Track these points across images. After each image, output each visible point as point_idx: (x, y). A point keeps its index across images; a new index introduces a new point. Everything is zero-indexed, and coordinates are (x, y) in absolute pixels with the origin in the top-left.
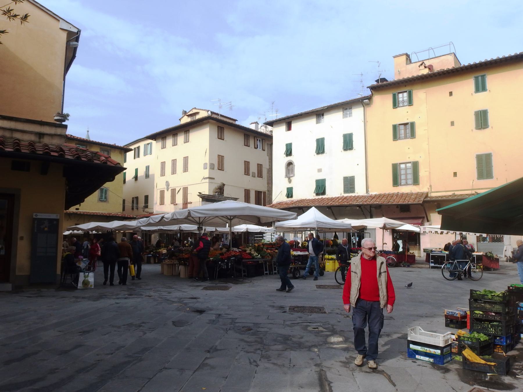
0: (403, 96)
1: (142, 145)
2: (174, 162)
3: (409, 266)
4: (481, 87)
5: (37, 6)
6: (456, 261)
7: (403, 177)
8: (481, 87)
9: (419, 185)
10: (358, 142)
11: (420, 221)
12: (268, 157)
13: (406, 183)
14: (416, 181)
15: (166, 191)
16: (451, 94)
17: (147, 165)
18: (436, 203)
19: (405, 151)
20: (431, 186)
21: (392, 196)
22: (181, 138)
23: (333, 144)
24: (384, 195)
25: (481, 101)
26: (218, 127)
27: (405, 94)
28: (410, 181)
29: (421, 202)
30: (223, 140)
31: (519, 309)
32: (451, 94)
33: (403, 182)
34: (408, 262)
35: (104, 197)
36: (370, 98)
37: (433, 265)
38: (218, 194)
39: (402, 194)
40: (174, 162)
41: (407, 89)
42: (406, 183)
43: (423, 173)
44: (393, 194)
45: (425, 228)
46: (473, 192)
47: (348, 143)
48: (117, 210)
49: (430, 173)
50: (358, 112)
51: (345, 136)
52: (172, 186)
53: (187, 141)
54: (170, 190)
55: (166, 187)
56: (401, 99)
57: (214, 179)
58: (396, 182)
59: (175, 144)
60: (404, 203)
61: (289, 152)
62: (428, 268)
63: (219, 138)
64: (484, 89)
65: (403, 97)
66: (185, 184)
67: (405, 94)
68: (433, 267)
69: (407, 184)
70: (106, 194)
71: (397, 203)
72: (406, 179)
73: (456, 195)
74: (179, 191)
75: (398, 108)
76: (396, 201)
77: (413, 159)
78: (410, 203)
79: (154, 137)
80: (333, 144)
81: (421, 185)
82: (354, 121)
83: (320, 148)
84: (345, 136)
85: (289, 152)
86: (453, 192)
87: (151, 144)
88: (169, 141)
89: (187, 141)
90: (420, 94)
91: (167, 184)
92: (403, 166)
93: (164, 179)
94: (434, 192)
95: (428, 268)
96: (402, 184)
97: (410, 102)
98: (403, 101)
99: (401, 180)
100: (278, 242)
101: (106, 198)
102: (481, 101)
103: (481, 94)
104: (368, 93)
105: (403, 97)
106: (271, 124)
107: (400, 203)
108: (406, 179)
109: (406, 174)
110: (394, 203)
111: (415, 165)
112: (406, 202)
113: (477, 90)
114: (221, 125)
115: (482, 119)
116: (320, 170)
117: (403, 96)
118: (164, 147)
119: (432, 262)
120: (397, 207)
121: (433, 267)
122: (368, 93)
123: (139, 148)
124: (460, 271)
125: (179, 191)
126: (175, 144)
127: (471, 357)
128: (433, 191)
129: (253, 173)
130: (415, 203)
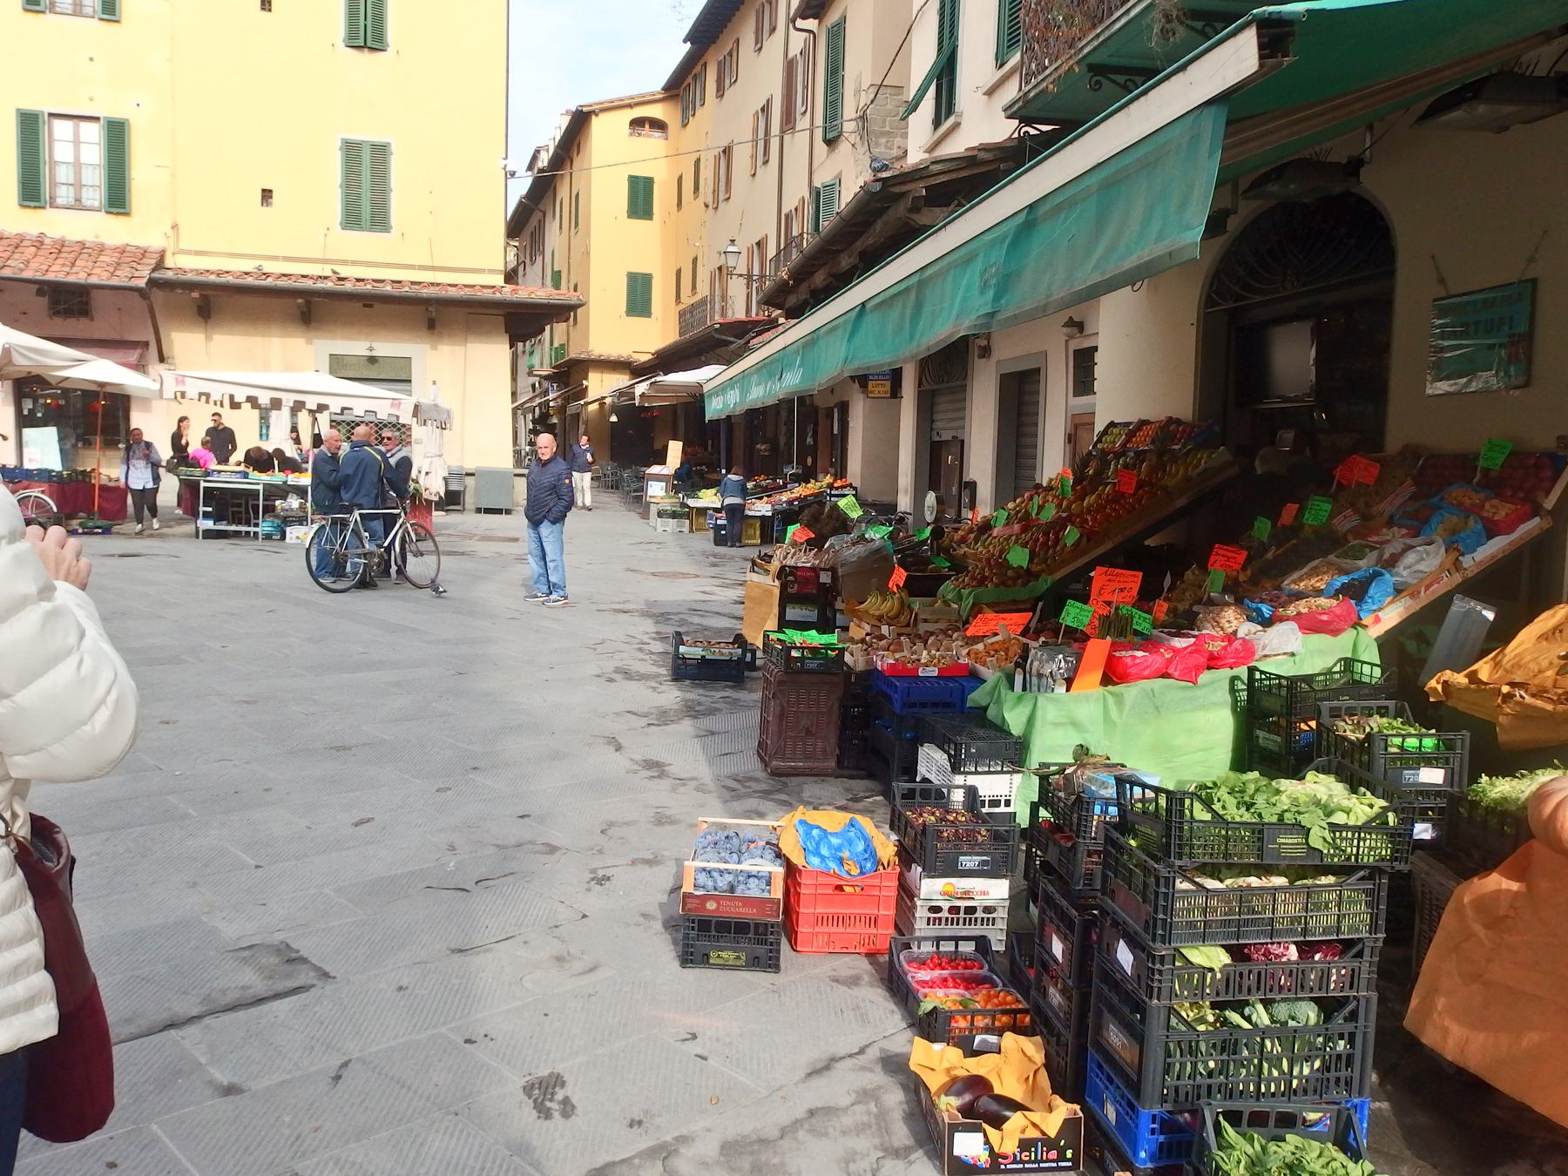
3: (107, 531)
6: (356, 514)
9: (127, 214)
11: (134, 356)
14: (117, 199)
18: (195, 295)
28: (95, 195)
29: (142, 283)
31: (1097, 809)
33: (64, 195)
34: (104, 514)
37: (209, 524)
38: (799, 785)
42: (78, 200)
44: (21, 238)
45: (181, 380)
46: (326, 270)
58: (32, 191)
60: (71, 279)
62: (188, 536)
68: (209, 535)
69: (78, 205)
71: (39, 276)
73: (268, 275)
76: (33, 265)
78: (94, 280)
86: (257, 263)
92: (62, 129)
94: (188, 252)
95: (188, 536)
96: (60, 201)
99: (54, 184)
107: (51, 277)
110: (28, 274)
112: (78, 276)
119: (206, 515)
120: (40, 293)
121: (209, 535)
124: (372, 554)
128: (183, 245)
130: (115, 282)
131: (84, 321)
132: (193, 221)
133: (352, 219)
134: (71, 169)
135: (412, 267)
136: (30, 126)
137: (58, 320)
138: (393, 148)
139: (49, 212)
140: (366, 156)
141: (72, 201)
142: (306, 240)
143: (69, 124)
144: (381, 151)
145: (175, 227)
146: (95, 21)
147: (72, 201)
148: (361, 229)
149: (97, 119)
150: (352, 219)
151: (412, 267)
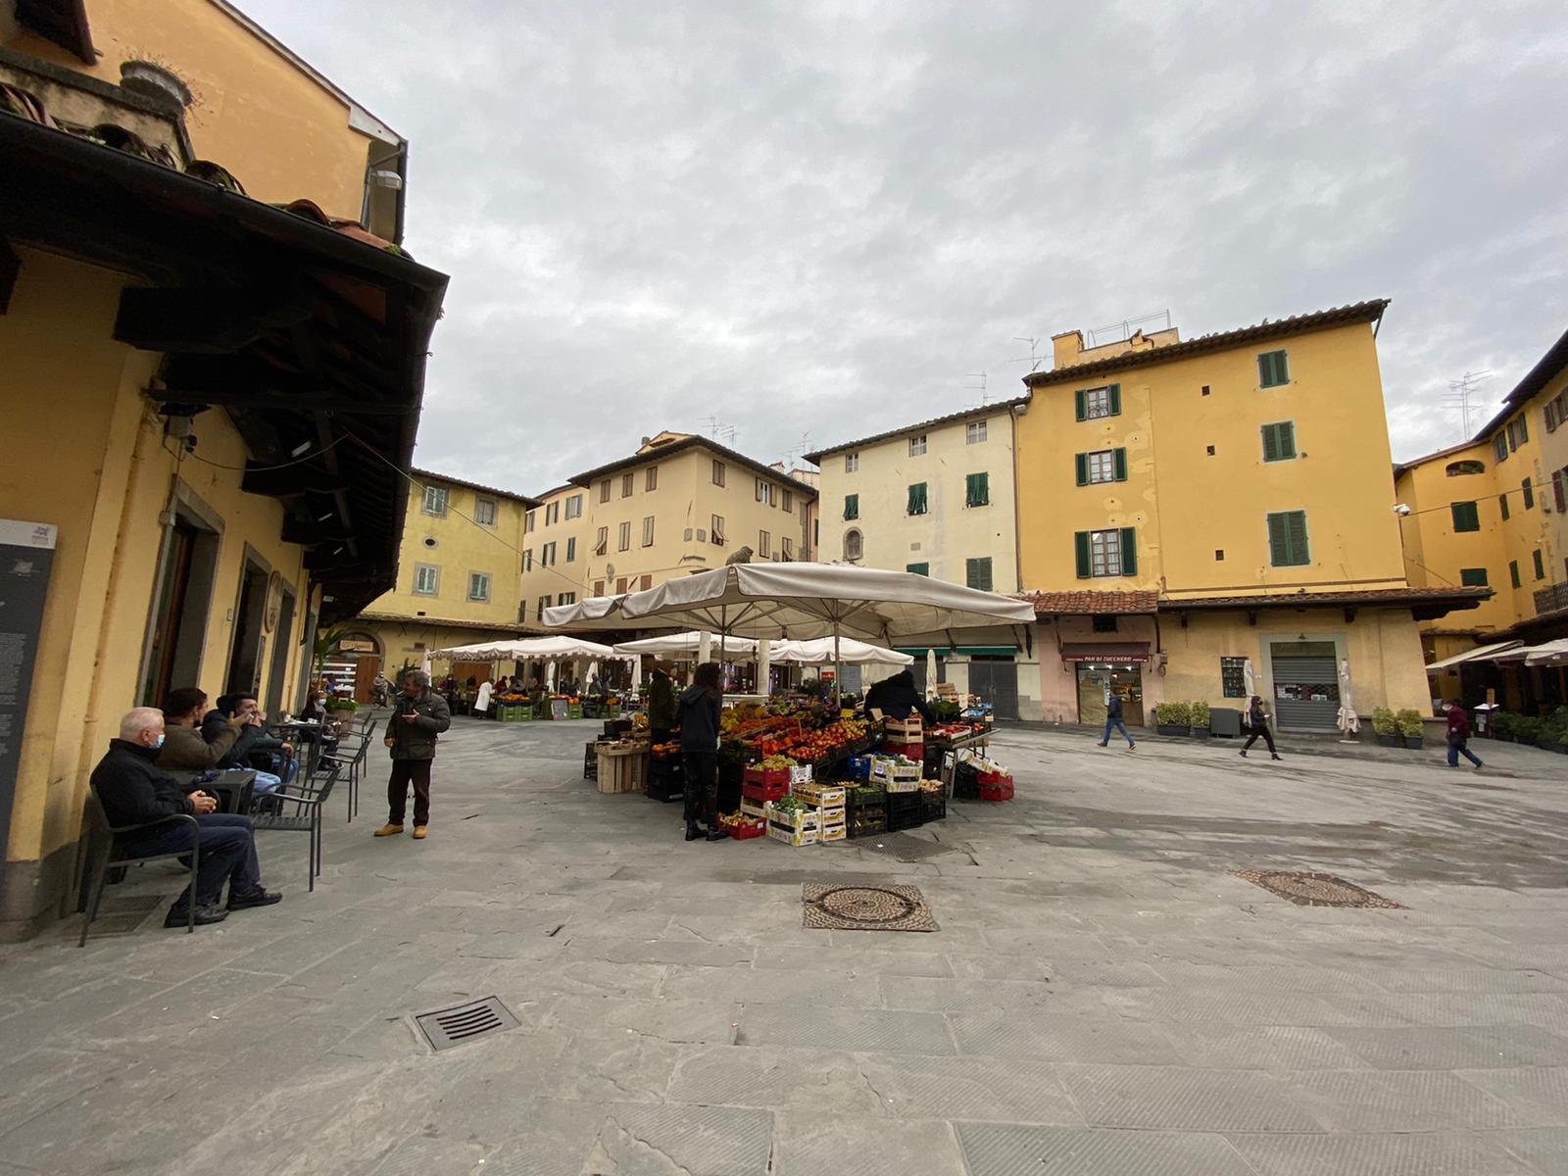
0: (1098, 396)
1: (562, 498)
2: (625, 527)
4: (1274, 373)
5: (268, 46)
7: (1099, 560)
8: (1274, 373)
10: (1000, 487)
12: (801, 527)
13: (1107, 571)
14: (1129, 567)
15: (606, 582)
16: (1206, 391)
17: (571, 536)
19: (1107, 508)
20: (1163, 579)
21: (1079, 596)
22: (640, 479)
23: (947, 493)
24: (1061, 596)
25: (1276, 405)
26: (714, 461)
27: (1103, 394)
30: (723, 487)
32: (1206, 391)
33: (1101, 570)
35: (479, 592)
36: (1026, 401)
39: (1101, 594)
40: (625, 527)
41: (1109, 381)
42: (1102, 478)
43: (1143, 551)
47: (977, 491)
48: (507, 618)
49: (1161, 552)
50: (999, 429)
51: (971, 479)
52: (619, 573)
53: (651, 486)
54: (615, 582)
55: (607, 576)
56: (1093, 404)
57: (704, 559)
58: (1084, 570)
59: (627, 492)
61: (851, 509)
63: (714, 483)
64: (1282, 379)
65: (1098, 400)
66: (645, 570)
67: (1103, 394)
69: (1107, 574)
70: (484, 586)
72: (1106, 564)
74: (632, 583)
75: (1088, 422)
77: (1120, 523)
79: (583, 481)
80: (947, 493)
81: (1140, 577)
82: (992, 452)
83: (917, 501)
84: (971, 479)
85: (851, 509)
87: (580, 497)
88: (617, 486)
89: (651, 486)
90: (1135, 389)
91: (610, 569)
92: (1095, 459)
93: (604, 561)
97: (1115, 409)
98: (1098, 408)
100: (929, 707)
101: (483, 593)
102: (1276, 405)
103: (1277, 391)
104: (1023, 392)
105: (1098, 400)
106: (815, 459)
108: (1106, 564)
109: (1106, 554)
111: (1128, 536)
113: (1267, 382)
114: (719, 458)
115: (1278, 442)
116: (916, 547)
117: (1098, 396)
118: (605, 499)
122: (1023, 392)
123: (557, 503)
125: (632, 583)
126: (627, 492)
127: (1061, 852)
128: (1168, 588)
129: (774, 554)
131: (1113, 633)
132: (1172, 571)
133: (1279, 559)
134: (1104, 461)
135: (1330, 584)
136: (1082, 540)
137: (1098, 634)
138: (1306, 513)
139: (1090, 486)
140: (1286, 522)
141: (1103, 573)
142: (1253, 573)
143: (1097, 456)
144: (1297, 518)
145: (1163, 579)
146: (1109, 417)
147: (1103, 573)
148: (1290, 514)
149: (1110, 451)
150: (1279, 559)
151: (1330, 584)
